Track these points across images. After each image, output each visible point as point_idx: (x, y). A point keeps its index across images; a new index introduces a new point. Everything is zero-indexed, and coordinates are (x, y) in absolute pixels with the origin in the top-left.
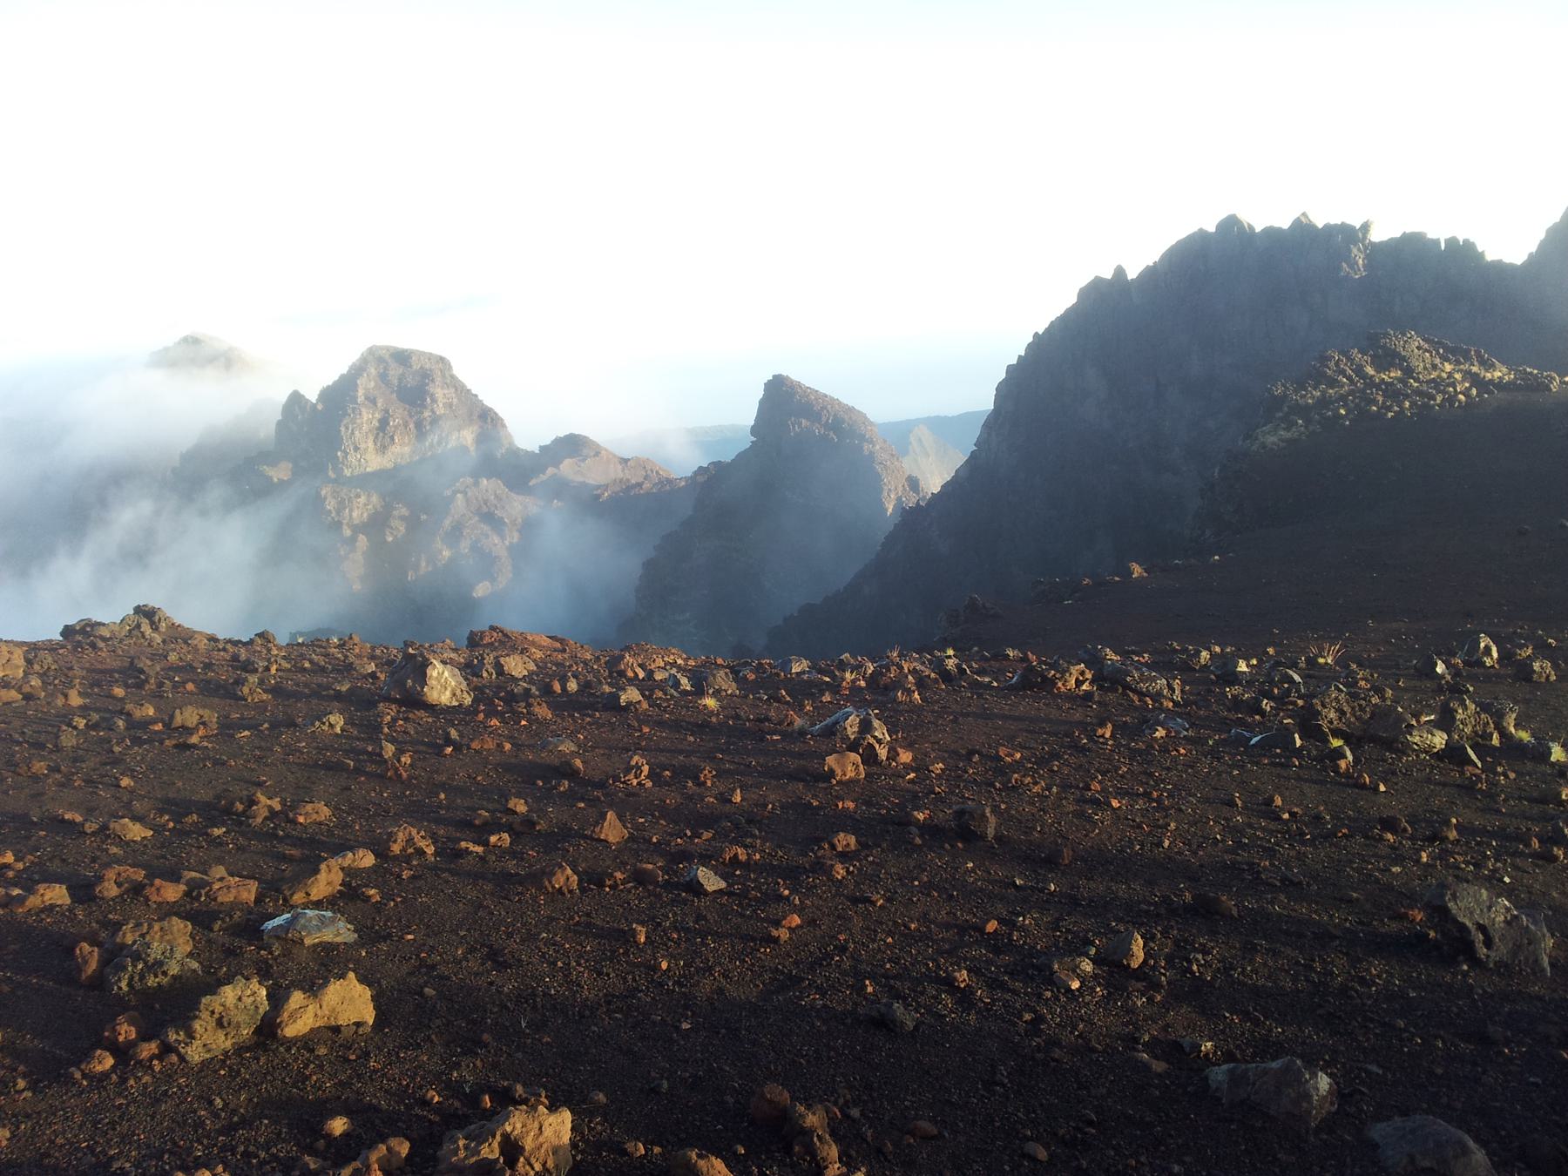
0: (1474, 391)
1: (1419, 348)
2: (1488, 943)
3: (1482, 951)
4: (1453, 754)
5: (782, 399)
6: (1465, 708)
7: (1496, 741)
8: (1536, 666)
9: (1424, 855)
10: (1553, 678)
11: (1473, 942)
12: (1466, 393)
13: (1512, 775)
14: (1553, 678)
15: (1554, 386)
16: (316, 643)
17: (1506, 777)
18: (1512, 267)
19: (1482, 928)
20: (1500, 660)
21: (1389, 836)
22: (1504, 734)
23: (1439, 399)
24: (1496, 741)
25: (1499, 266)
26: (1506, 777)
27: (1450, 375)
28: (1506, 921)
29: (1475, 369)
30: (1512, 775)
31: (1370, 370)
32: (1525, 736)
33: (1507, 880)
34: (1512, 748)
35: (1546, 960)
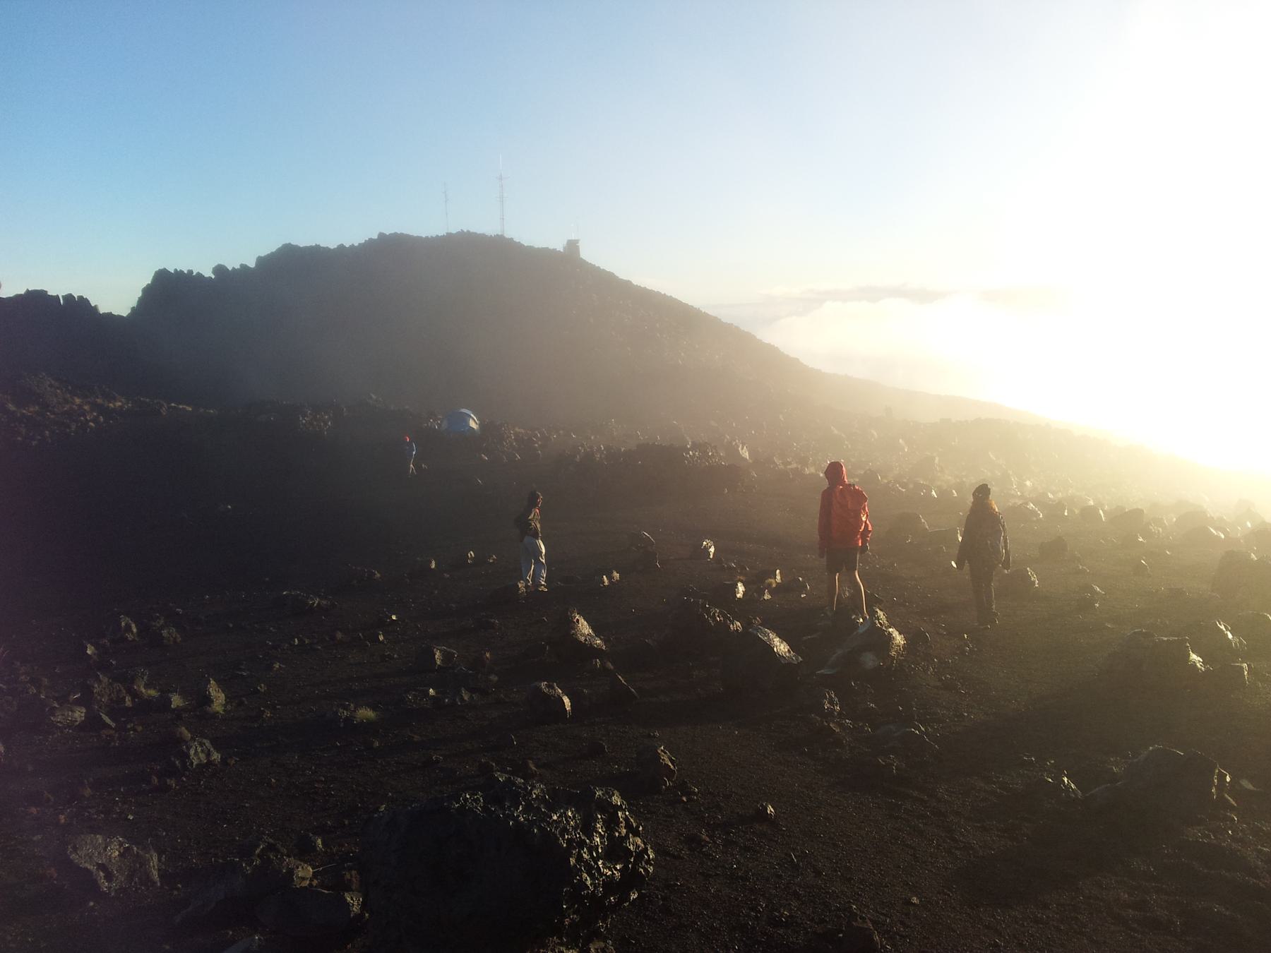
0: (102, 419)
1: (51, 386)
2: (109, 877)
3: (105, 885)
4: (92, 722)
5: (573, 246)
6: (100, 682)
7: (128, 703)
8: (165, 633)
9: (62, 817)
10: (179, 640)
11: (96, 881)
12: (95, 420)
13: (140, 729)
14: (179, 640)
15: (164, 411)
16: (1138, 513)
17: (135, 730)
18: (120, 317)
19: (102, 867)
20: (140, 631)
21: (34, 810)
22: (135, 695)
23: (74, 427)
24: (128, 703)
25: (109, 316)
26: (135, 730)
27: (80, 406)
28: (121, 855)
29: (99, 401)
30: (140, 729)
31: (11, 407)
32: (152, 692)
33: (131, 817)
34: (145, 706)
35: (155, 873)
